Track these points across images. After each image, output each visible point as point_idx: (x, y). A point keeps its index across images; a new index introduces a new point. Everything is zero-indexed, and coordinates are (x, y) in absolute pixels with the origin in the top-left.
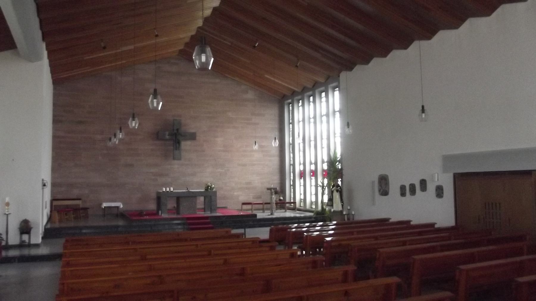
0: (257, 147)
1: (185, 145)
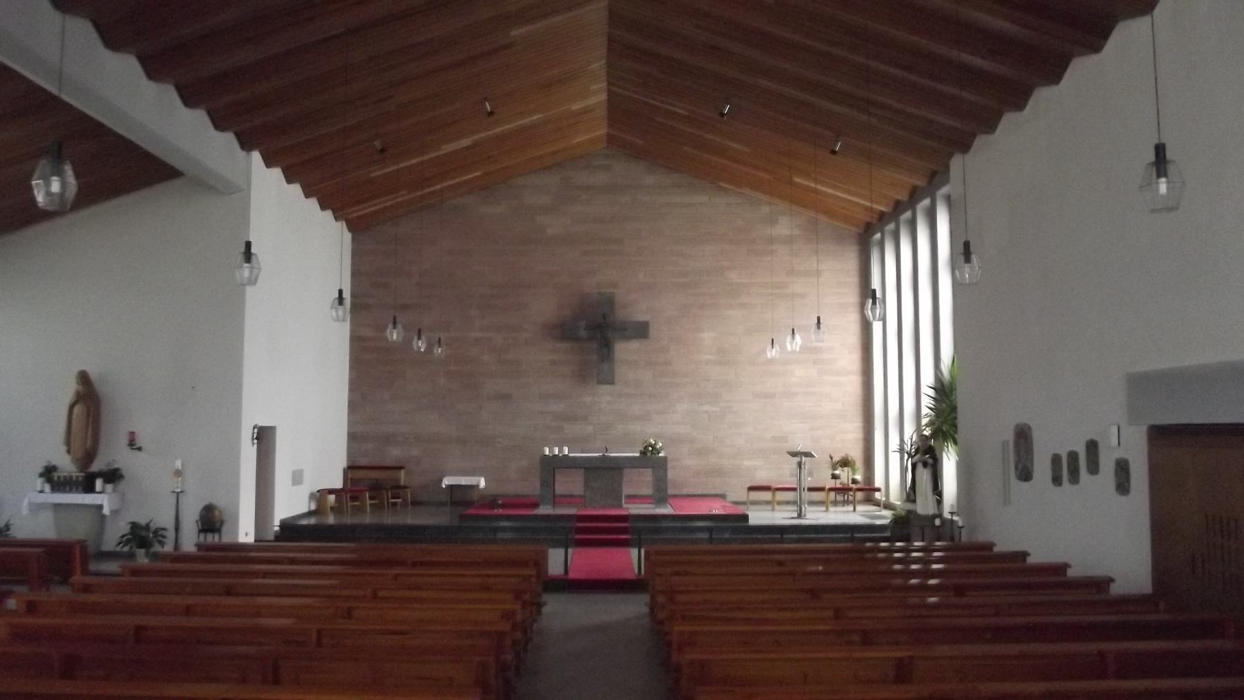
0: (776, 351)
1: (624, 350)
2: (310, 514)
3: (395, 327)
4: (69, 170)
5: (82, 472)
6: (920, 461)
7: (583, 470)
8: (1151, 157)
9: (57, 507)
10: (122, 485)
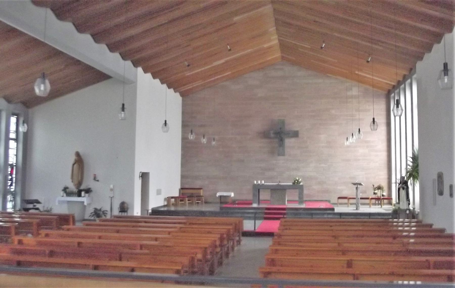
1: (289, 142)
2: (164, 206)
3: (192, 134)
4: (47, 82)
5: (77, 189)
6: (401, 187)
7: (269, 190)
8: (442, 68)
9: (69, 202)
10: (92, 194)
